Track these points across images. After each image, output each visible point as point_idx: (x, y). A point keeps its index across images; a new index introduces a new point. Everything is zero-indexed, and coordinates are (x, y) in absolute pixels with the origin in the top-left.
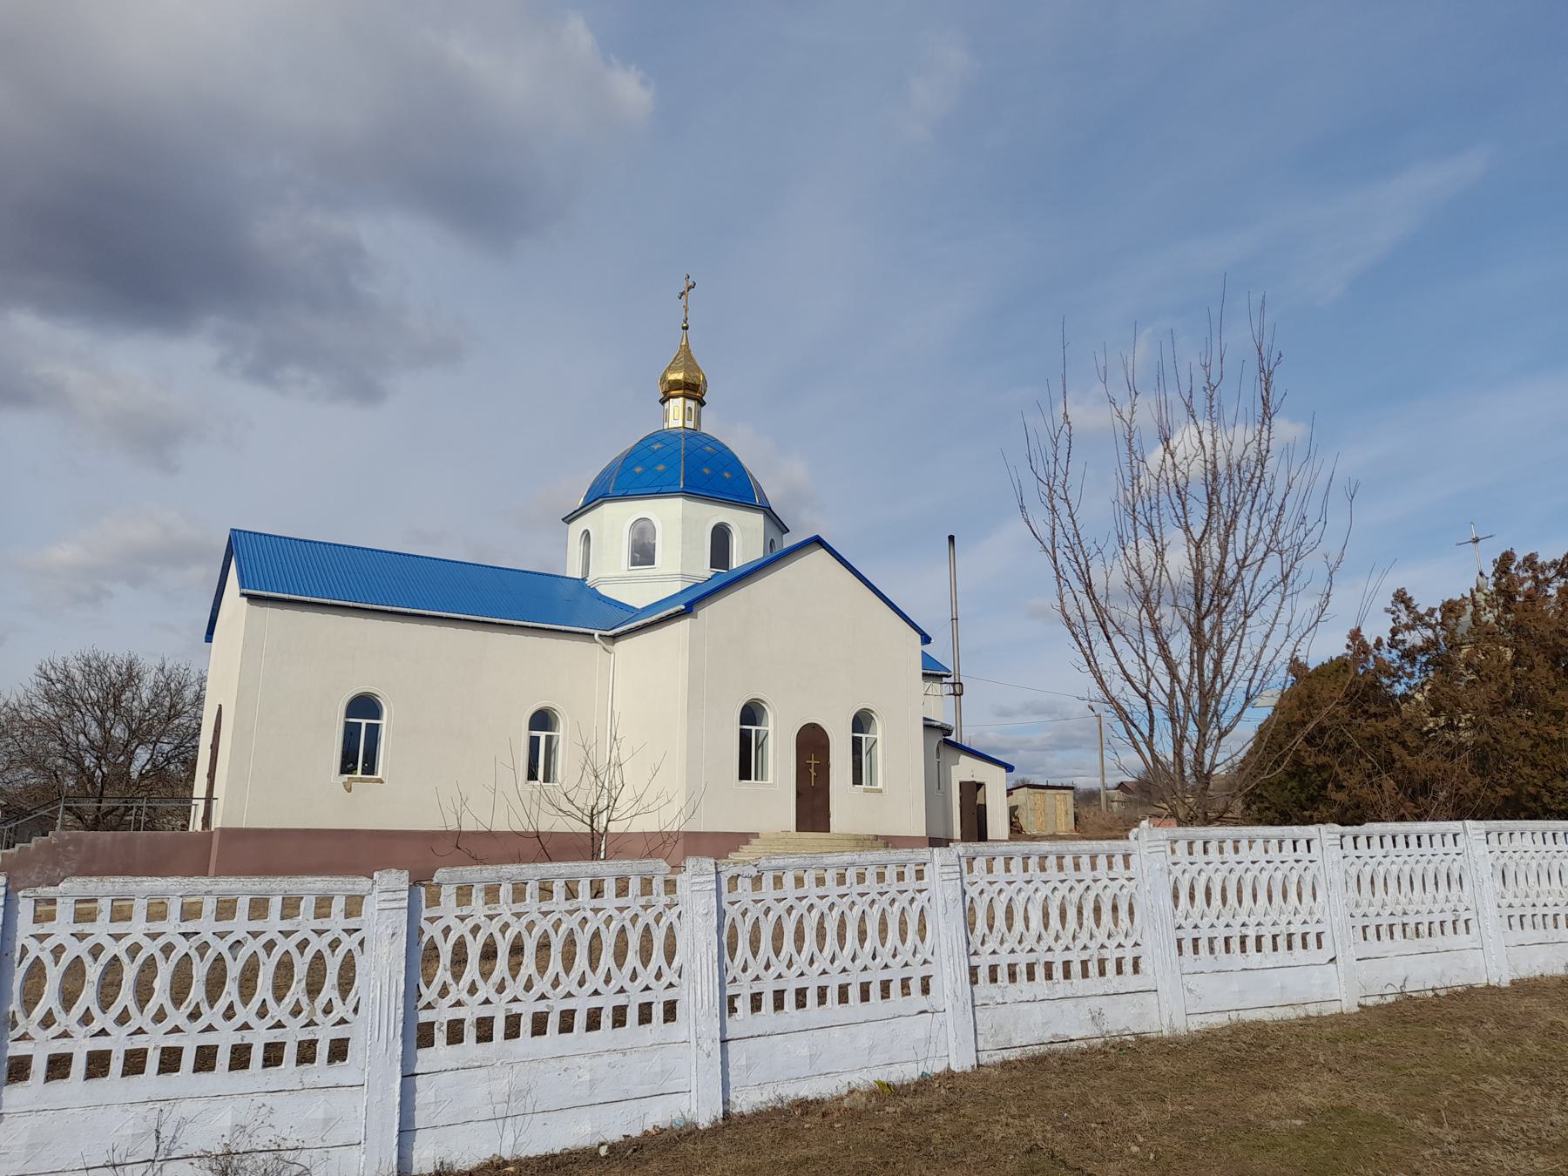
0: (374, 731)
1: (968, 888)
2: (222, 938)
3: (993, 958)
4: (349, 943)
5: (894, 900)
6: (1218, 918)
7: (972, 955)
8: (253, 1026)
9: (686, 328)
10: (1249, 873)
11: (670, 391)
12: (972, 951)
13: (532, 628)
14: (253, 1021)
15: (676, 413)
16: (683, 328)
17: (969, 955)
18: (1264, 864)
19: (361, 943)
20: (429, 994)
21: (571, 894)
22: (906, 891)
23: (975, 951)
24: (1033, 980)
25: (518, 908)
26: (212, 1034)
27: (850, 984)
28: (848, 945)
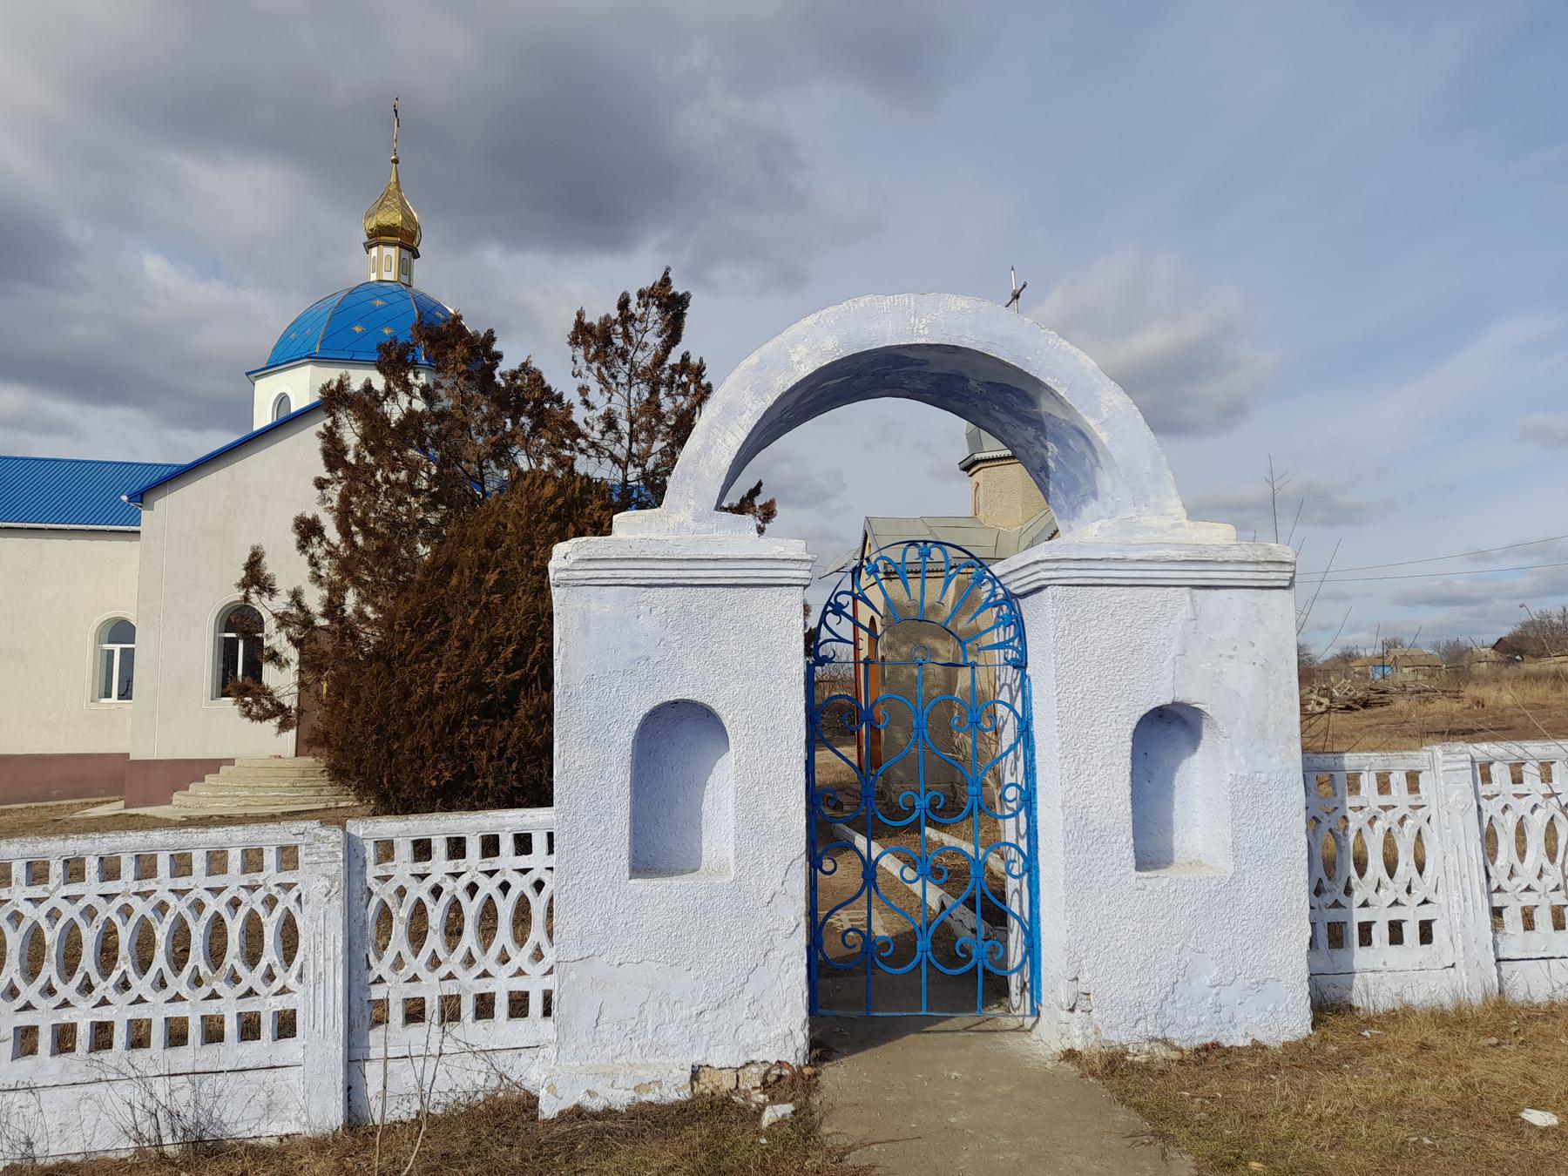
0: (128, 656)
1: (1483, 803)
2: (386, 881)
3: (480, 985)
4: (286, 901)
5: (1404, 818)
6: (1539, 877)
7: (1495, 891)
8: (222, 995)
9: (396, 161)
10: (1508, 813)
11: (379, 236)
12: (1494, 887)
13: (111, 531)
14: (423, 973)
15: (383, 264)
16: (393, 161)
17: (1490, 893)
18: (1539, 800)
19: (299, 899)
20: (381, 968)
21: (1384, 786)
22: (1423, 806)
23: (1499, 887)
24: (1369, 944)
25: (216, 881)
26: (486, 980)
27: (1536, 906)
28: (1530, 855)
